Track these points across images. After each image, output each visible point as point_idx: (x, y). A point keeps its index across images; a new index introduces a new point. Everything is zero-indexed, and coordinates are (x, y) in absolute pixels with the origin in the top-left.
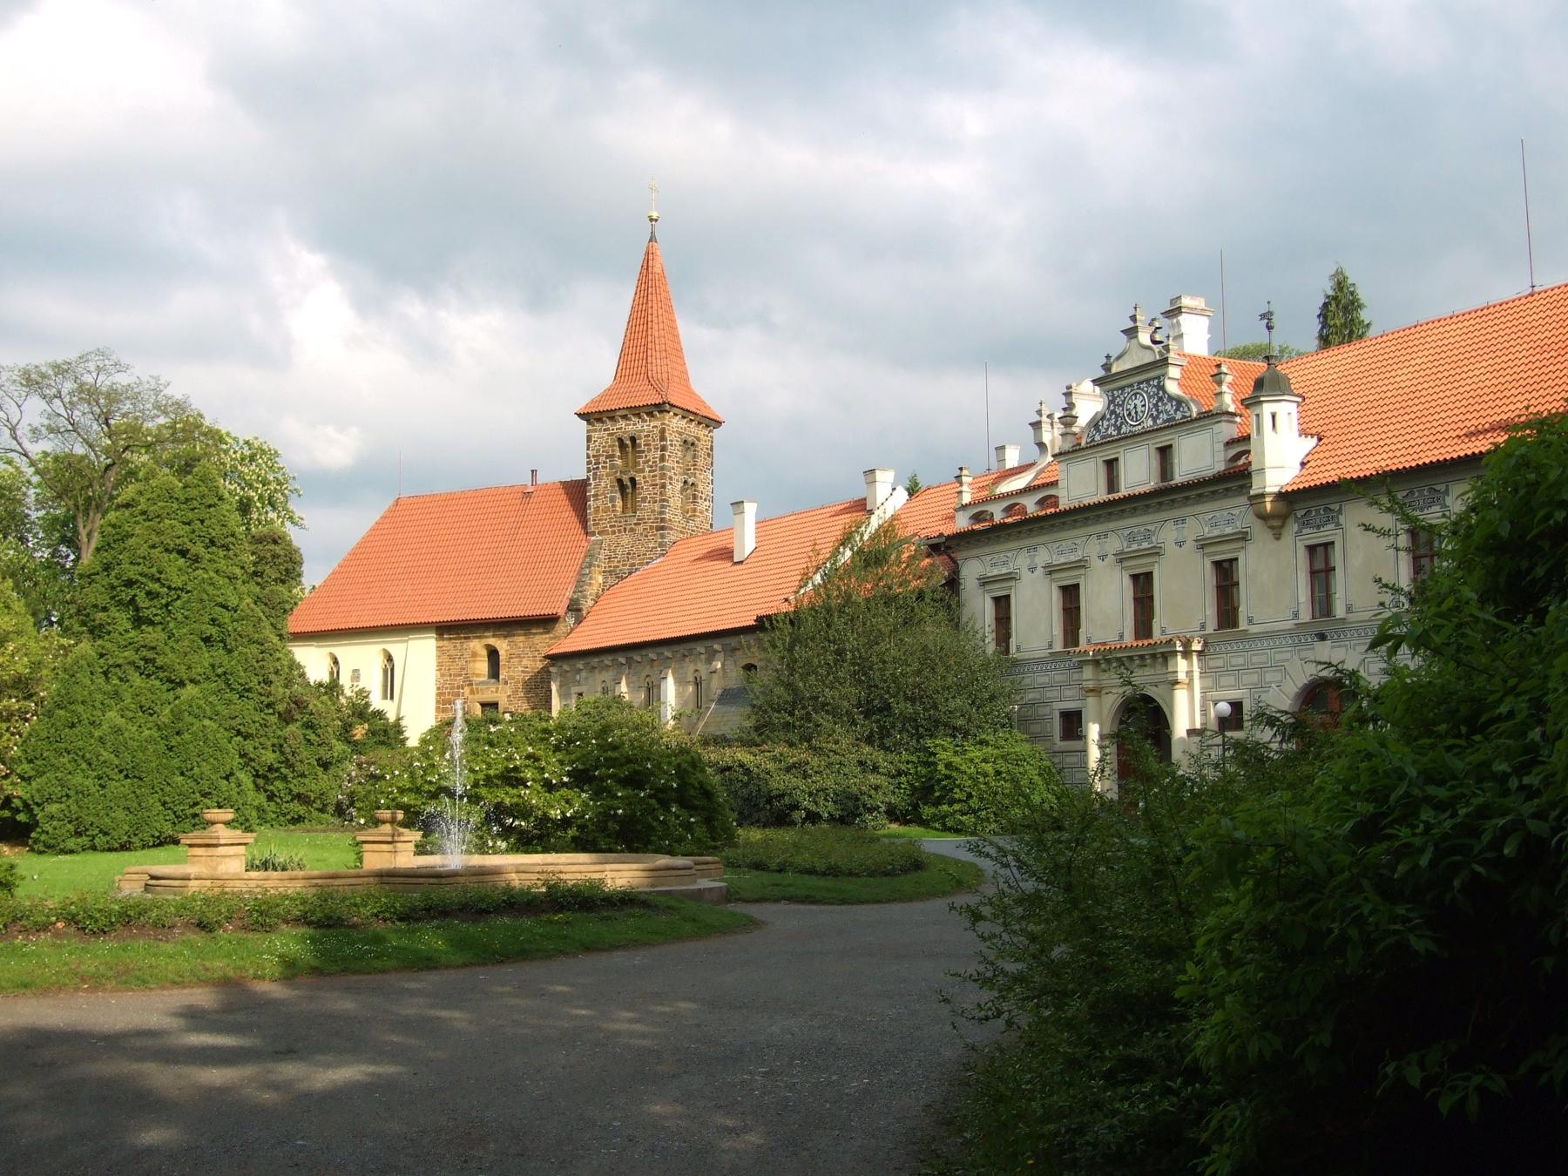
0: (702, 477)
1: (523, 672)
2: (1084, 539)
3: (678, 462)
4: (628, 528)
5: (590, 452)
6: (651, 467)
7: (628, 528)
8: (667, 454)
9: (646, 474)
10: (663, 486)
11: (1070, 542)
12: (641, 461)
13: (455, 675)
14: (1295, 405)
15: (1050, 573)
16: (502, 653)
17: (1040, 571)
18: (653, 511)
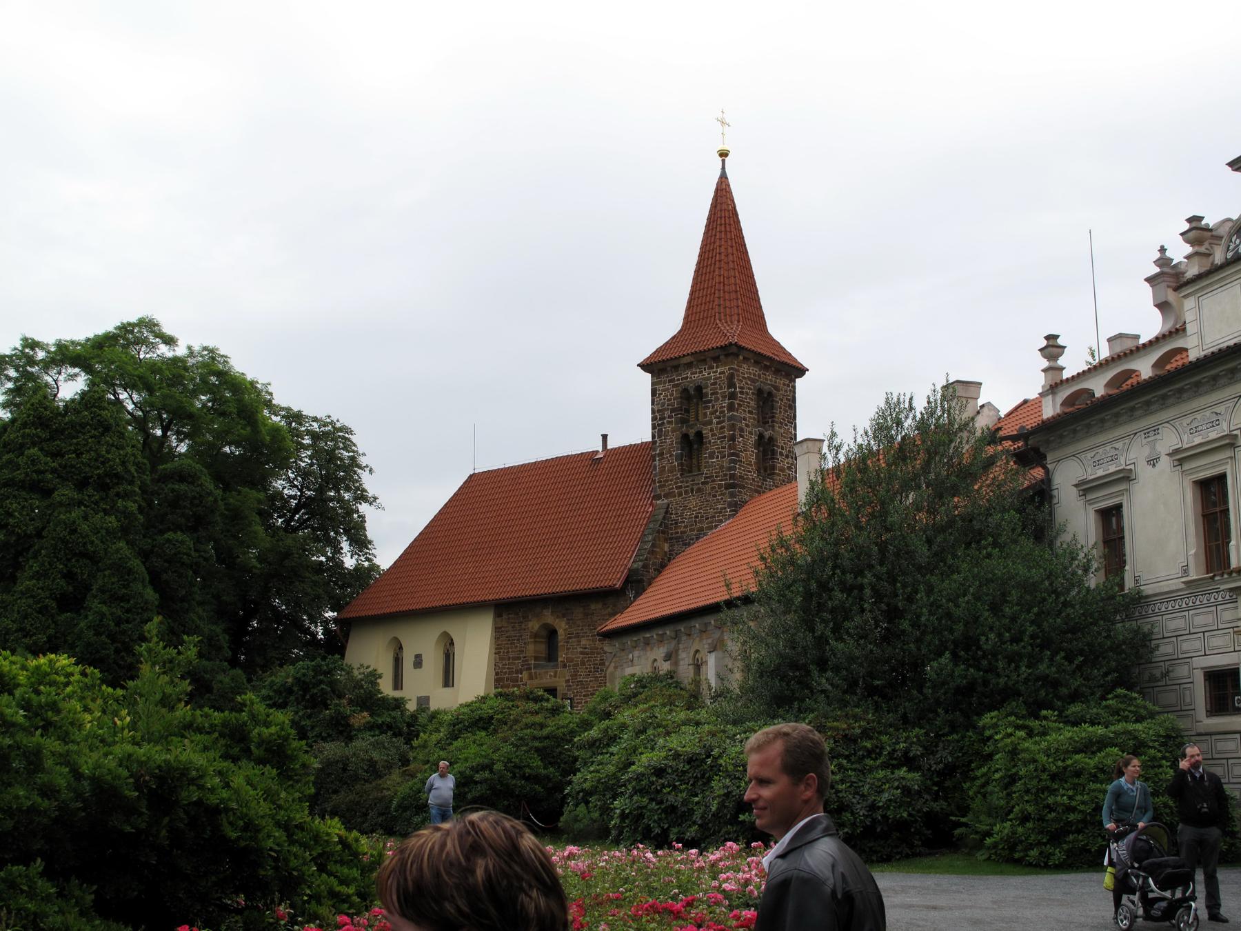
0: (782, 431)
1: (582, 653)
2: (1231, 405)
3: (750, 412)
4: (695, 488)
6: (719, 418)
7: (695, 488)
8: (736, 402)
9: (714, 426)
10: (733, 438)
11: (1208, 413)
12: (708, 412)
13: (514, 659)
15: (1181, 462)
16: (560, 632)
17: (1165, 462)
18: (722, 467)
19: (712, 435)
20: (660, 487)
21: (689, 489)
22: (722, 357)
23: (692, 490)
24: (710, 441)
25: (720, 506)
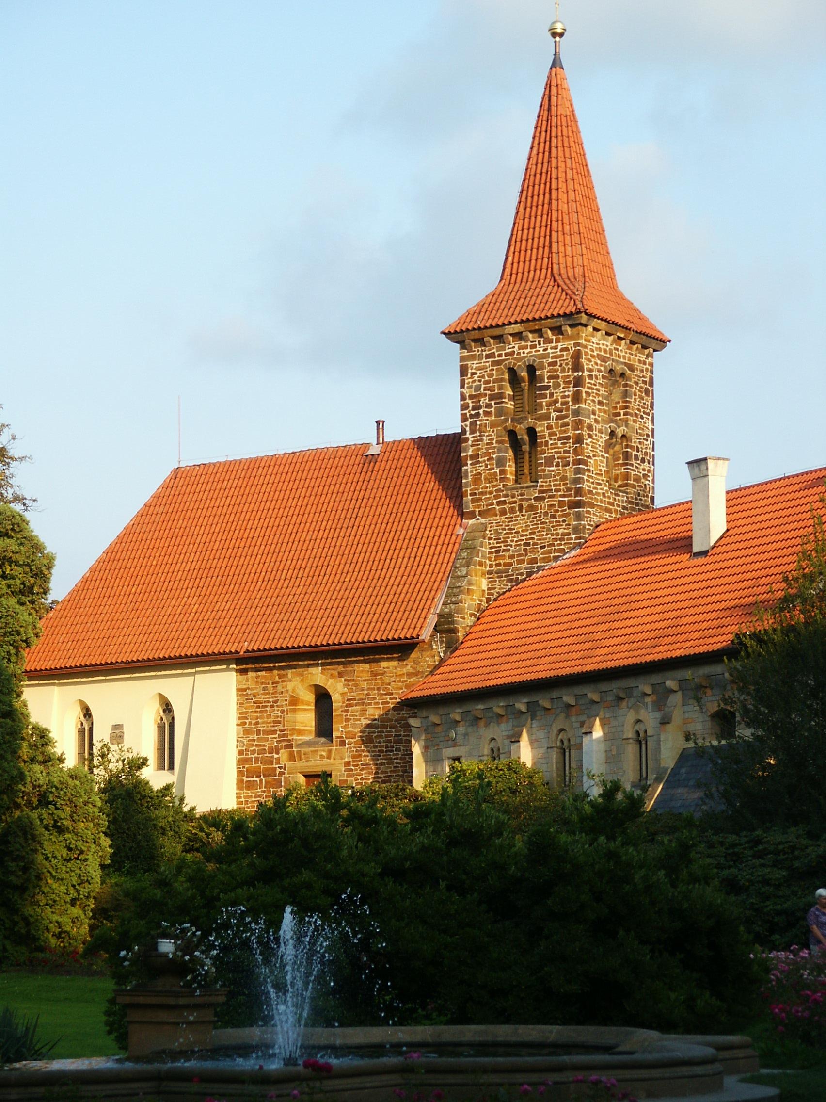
9: (552, 422)
20: (473, 501)
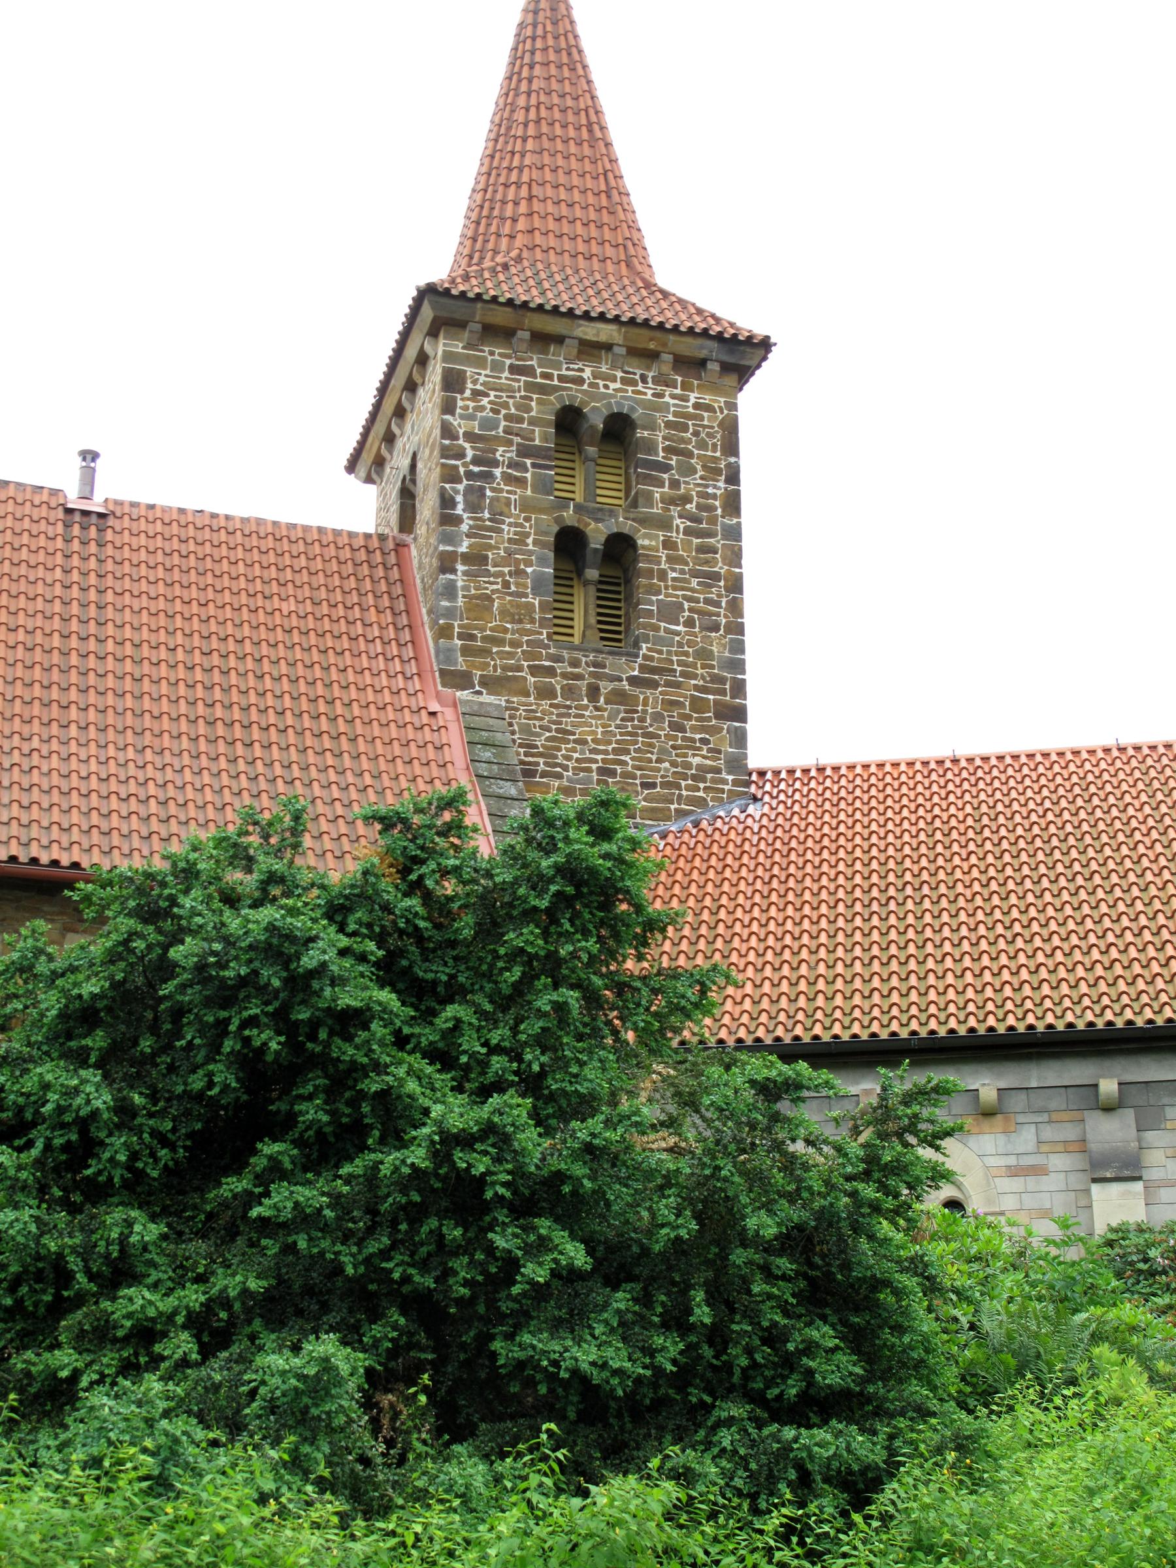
5: (455, 421)
7: (606, 687)
12: (657, 493)
14: (1033, 1128)
19: (670, 559)
21: (583, 685)
22: (713, 366)
23: (594, 692)
24: (663, 575)
25: (696, 761)
